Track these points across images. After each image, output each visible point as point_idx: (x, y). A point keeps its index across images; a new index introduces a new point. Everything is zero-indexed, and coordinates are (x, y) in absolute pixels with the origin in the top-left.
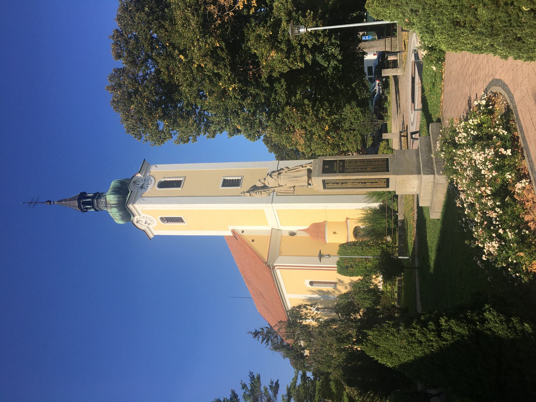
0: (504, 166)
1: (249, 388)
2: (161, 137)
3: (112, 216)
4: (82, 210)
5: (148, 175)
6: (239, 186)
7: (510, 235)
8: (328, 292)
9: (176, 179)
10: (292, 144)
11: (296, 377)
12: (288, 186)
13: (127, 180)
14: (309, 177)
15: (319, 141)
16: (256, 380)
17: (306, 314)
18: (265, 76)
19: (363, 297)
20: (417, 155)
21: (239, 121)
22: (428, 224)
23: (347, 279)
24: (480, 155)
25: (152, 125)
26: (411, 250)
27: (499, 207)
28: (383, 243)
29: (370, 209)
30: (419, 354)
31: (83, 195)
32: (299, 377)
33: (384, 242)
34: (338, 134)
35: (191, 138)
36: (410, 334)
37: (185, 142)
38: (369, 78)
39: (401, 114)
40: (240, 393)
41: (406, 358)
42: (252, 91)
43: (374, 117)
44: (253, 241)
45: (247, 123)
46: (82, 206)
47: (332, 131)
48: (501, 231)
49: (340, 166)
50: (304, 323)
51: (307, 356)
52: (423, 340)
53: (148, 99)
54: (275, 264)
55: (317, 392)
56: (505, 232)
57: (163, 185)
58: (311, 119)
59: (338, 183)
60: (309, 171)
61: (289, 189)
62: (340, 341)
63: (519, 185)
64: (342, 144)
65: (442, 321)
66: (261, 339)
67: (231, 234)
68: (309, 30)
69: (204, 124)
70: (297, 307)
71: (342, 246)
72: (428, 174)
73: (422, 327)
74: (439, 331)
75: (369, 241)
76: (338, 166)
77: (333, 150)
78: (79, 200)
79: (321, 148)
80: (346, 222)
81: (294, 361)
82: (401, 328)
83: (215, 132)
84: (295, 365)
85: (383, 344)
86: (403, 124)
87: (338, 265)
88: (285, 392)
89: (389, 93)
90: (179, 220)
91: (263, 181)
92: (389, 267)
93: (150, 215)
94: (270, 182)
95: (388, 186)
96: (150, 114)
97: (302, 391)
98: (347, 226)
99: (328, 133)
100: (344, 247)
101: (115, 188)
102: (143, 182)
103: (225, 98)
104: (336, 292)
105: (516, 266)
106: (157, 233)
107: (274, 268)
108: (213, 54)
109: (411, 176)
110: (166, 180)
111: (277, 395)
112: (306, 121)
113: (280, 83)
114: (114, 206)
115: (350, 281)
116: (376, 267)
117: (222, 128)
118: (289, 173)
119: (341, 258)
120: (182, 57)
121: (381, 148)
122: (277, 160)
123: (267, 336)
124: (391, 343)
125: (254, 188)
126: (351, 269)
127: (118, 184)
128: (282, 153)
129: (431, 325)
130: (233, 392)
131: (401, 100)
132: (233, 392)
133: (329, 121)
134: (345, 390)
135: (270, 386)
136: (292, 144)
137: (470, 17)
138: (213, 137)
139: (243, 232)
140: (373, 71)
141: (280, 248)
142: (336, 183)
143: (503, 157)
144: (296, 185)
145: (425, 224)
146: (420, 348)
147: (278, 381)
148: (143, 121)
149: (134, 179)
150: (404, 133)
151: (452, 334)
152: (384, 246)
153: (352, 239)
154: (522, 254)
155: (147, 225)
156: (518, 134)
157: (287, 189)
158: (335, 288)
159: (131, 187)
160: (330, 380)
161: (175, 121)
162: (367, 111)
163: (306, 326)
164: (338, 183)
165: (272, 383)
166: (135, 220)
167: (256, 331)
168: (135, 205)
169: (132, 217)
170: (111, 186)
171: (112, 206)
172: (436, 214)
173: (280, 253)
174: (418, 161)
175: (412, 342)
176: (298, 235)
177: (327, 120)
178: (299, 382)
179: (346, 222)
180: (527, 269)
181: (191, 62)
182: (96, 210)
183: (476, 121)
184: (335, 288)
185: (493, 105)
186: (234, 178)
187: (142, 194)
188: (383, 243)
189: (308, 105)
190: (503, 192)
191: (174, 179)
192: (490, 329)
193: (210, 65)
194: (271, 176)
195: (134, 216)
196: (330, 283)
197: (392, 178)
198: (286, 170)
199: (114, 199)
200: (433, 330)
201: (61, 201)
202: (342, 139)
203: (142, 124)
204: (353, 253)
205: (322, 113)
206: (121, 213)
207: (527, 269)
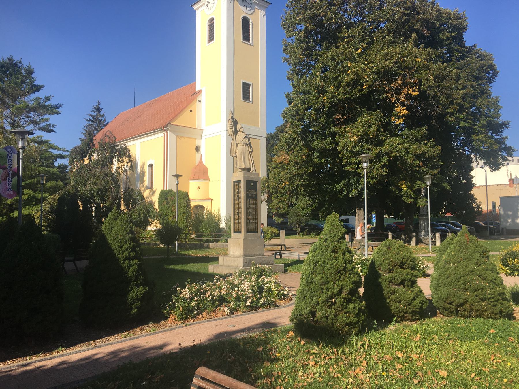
0: (240, 302)
1: (46, 104)
2: (289, 27)
5: (256, 7)
7: (193, 303)
8: (143, 181)
9: (251, 36)
10: (278, 151)
11: (59, 150)
12: (237, 152)
14: (243, 170)
16: (54, 111)
17: (123, 161)
18: (336, 129)
19: (141, 212)
20: (259, 255)
22: (205, 265)
23: (155, 199)
24: (247, 287)
25: (300, 19)
26: (183, 253)
27: (213, 298)
28: (189, 230)
29: (219, 220)
30: (113, 246)
32: (60, 152)
33: (191, 232)
34: (287, 192)
35: (288, 56)
36: (126, 241)
37: (284, 50)
41: (110, 238)
43: (303, 224)
44: (191, 111)
48: (196, 299)
49: (252, 194)
50: (114, 160)
51: (84, 161)
52: (123, 249)
53: (325, 16)
54: (168, 132)
55: (46, 169)
56: (195, 301)
57: (246, 22)
58: (295, 170)
59: (238, 193)
60: (249, 170)
61: (234, 153)
62: (99, 191)
63: (226, 309)
64: (278, 196)
65: (136, 261)
66: (93, 114)
67: (197, 89)
68: (365, 171)
69: (301, 69)
70: (129, 154)
71: (187, 195)
72: (243, 262)
73: (131, 248)
74: (130, 258)
75: (191, 218)
77: (273, 188)
79: (275, 178)
80: (209, 199)
81: (78, 149)
82: (130, 235)
83: (292, 80)
84: (75, 150)
85: (118, 223)
86: (293, 248)
87: (169, 190)
88: (44, 139)
90: (211, 38)
91: (241, 130)
92: (168, 234)
94: (240, 137)
95: (235, 232)
96: (310, 18)
97: (47, 154)
98: (205, 199)
100: (185, 197)
105: (173, 307)
106: (198, 13)
108: (356, 83)
109: (242, 250)
110: (251, 26)
111: (41, 131)
115: (153, 201)
116: (167, 224)
117: (295, 87)
118: (247, 153)
119: (175, 193)
120: (360, 50)
121: (272, 229)
122: (268, 135)
123: (97, 120)
124: (120, 228)
125: (234, 123)
126: (165, 203)
128: (272, 140)
129: (133, 254)
130: (42, 87)
132: (42, 87)
134: (51, 195)
135: (50, 124)
136: (278, 151)
137: (318, 270)
138: (288, 78)
139: (200, 101)
141: (184, 137)
142: (239, 192)
143: (246, 301)
145: (205, 262)
146: (117, 247)
147: (55, 132)
148: (303, 11)
150: (283, 248)
151: (128, 267)
152: (187, 232)
153: (193, 204)
154: (181, 309)
155: (206, 3)
156: (261, 310)
158: (147, 188)
160: (57, 181)
161: (302, 42)
163: (112, 163)
164: (238, 193)
165: (53, 126)
172: (211, 268)
173: (179, 137)
174: (254, 255)
175: (121, 242)
176: (197, 155)
178: (55, 152)
179: (209, 199)
180: (171, 313)
181: (353, 60)
183: (273, 288)
184: (147, 188)
185: (284, 299)
186: (251, 94)
188: (189, 230)
190: (222, 301)
191: (251, 34)
192: (132, 289)
193: (347, 79)
194: (246, 137)
196: (152, 183)
197: (242, 235)
198: (250, 150)
200: (129, 255)
203: (301, 9)
204: (180, 204)
206: (168, 353)
207: (171, 313)
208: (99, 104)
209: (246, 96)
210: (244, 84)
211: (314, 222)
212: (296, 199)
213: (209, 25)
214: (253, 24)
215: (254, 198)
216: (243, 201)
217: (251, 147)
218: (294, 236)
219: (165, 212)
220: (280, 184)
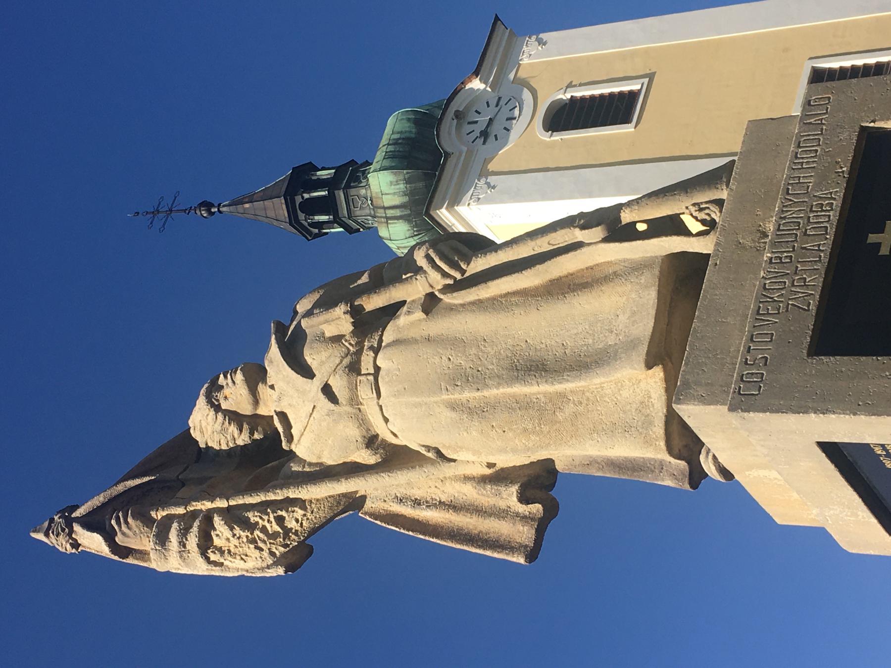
4: (303, 230)
5: (512, 76)
31: (302, 177)
46: (302, 216)
57: (567, 116)
60: (684, 279)
61: (485, 497)
78: (289, 196)
102: (493, 109)
110: (579, 93)
114: (398, 212)
127: (406, 126)
144: (567, 455)
149: (458, 104)
157: (469, 493)
159: (449, 138)
168: (461, 209)
170: (384, 140)
171: (390, 213)
182: (349, 230)
187: (487, 161)
199: (393, 189)
201: (241, 202)
214: (570, 86)
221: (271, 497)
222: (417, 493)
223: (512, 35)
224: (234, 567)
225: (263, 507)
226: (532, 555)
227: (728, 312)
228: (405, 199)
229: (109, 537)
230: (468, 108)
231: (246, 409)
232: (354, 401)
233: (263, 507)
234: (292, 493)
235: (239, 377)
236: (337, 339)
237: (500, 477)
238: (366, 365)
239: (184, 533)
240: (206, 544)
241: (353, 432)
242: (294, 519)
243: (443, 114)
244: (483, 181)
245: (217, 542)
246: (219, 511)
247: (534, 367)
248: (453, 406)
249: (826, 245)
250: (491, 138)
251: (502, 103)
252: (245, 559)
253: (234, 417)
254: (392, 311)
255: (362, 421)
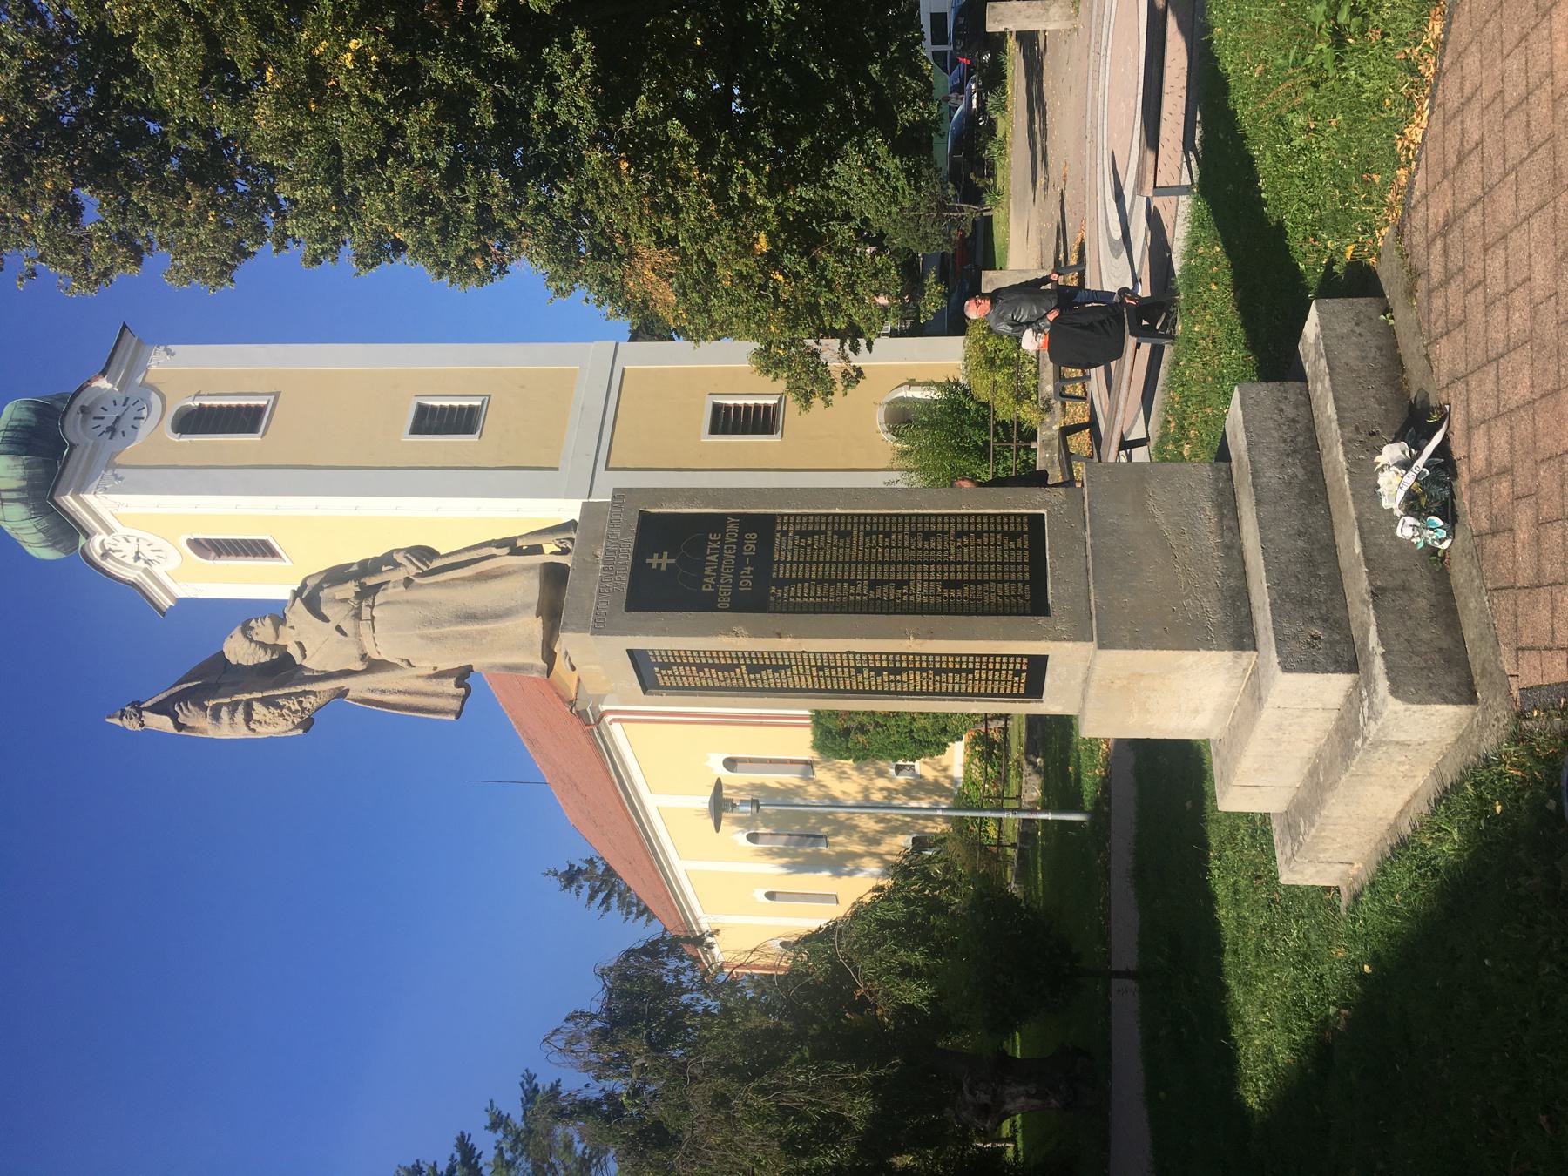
3: (12, 533)
5: (139, 380)
6: (473, 432)
12: (426, 667)
13: (62, 398)
15: (740, 290)
21: (389, 209)
34: (813, 262)
38: (934, 54)
39: (1054, 194)
40: (486, 1145)
42: (439, 71)
43: (951, 192)
45: (423, 213)
47: (791, 252)
54: (603, 708)
57: (194, 421)
59: (731, 668)
60: (555, 577)
61: (434, 686)
66: (586, 891)
72: (1312, 667)
76: (729, 555)
86: (1062, 231)
89: (1002, 107)
90: (260, 549)
93: (151, 530)
95: (1035, 689)
99: (773, 259)
101: (13, 429)
103: (317, 102)
104: (812, 789)
106: (184, 591)
107: (599, 720)
109: (1190, 657)
110: (207, 403)
112: (676, 213)
113: (567, 46)
114: (14, 495)
118: (434, 593)
126: (861, 738)
127: (25, 415)
131: (1054, 135)
133: (769, 216)
140: (950, 28)
144: (478, 662)
155: (141, 564)
159: (73, 428)
162: (925, 171)
164: (731, 668)
166: (95, 547)
167: (571, 866)
169: (82, 541)
177: (764, 209)
187: (114, 455)
189: (684, 147)
195: (87, 536)
196: (792, 762)
202: (829, 283)
205: (749, 183)
208: (555, 874)
209: (462, 421)
210: (417, 429)
211: (943, 148)
212: (847, 217)
213: (219, 554)
214: (198, 395)
215: (766, 543)
216: (787, 644)
217: (388, 560)
218: (997, 230)
219: (896, 738)
220: (775, 291)
221: (293, 690)
222: (383, 687)
223: (140, 342)
224: (263, 732)
225: (288, 696)
226: (458, 715)
227: (580, 594)
228: (24, 483)
229: (174, 717)
230: (93, 405)
231: (270, 640)
232: (357, 635)
233: (288, 696)
234: (308, 688)
235: (268, 621)
236: (345, 601)
237: (440, 675)
238: (366, 613)
239: (233, 712)
240: (248, 718)
241: (356, 652)
242: (310, 703)
243: (68, 407)
244: (110, 472)
245: (255, 717)
246: (257, 700)
247: (471, 617)
248: (422, 637)
249: (629, 563)
250: (119, 434)
251: (130, 402)
252: (272, 725)
253: (262, 645)
254: (377, 588)
255: (361, 647)
